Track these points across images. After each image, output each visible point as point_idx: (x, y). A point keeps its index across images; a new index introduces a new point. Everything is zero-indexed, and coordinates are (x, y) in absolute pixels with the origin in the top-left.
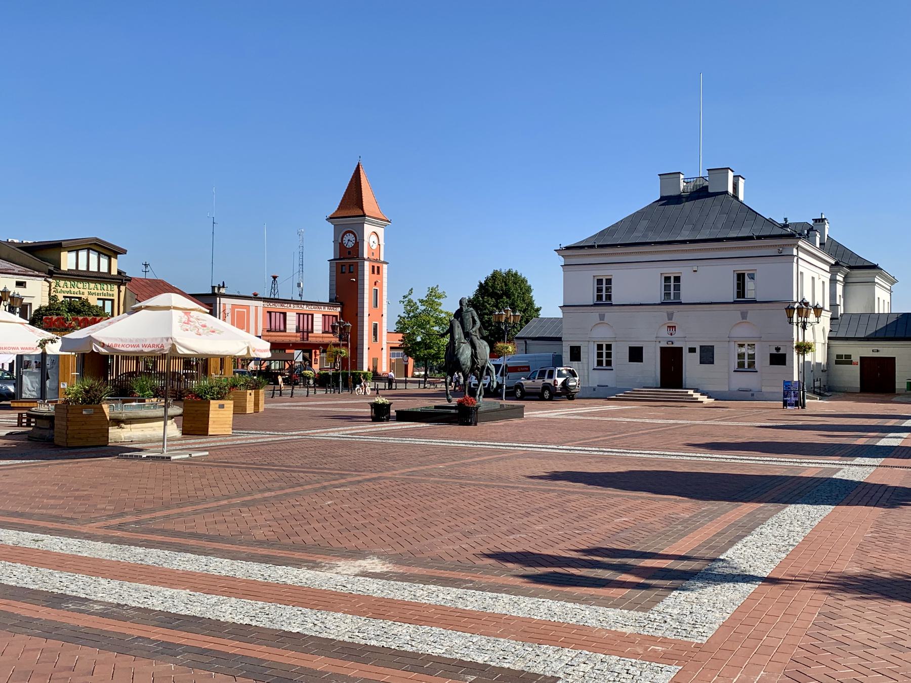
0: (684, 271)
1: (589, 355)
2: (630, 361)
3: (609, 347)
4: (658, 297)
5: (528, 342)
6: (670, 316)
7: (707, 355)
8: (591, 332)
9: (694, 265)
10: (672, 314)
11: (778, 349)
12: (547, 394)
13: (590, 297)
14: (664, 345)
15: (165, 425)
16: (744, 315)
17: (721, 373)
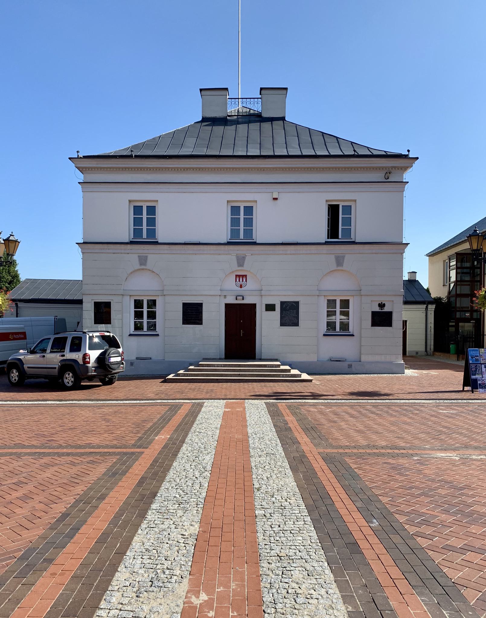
0: (260, 200)
1: (123, 319)
2: (184, 323)
3: (152, 303)
4: (223, 234)
5: (20, 304)
6: (241, 261)
7: (290, 313)
8: (131, 281)
9: (275, 191)
10: (244, 258)
11: (382, 306)
12: (69, 379)
13: (123, 230)
14: (231, 300)
15: (427, 308)
16: (339, 261)
17: (308, 338)
